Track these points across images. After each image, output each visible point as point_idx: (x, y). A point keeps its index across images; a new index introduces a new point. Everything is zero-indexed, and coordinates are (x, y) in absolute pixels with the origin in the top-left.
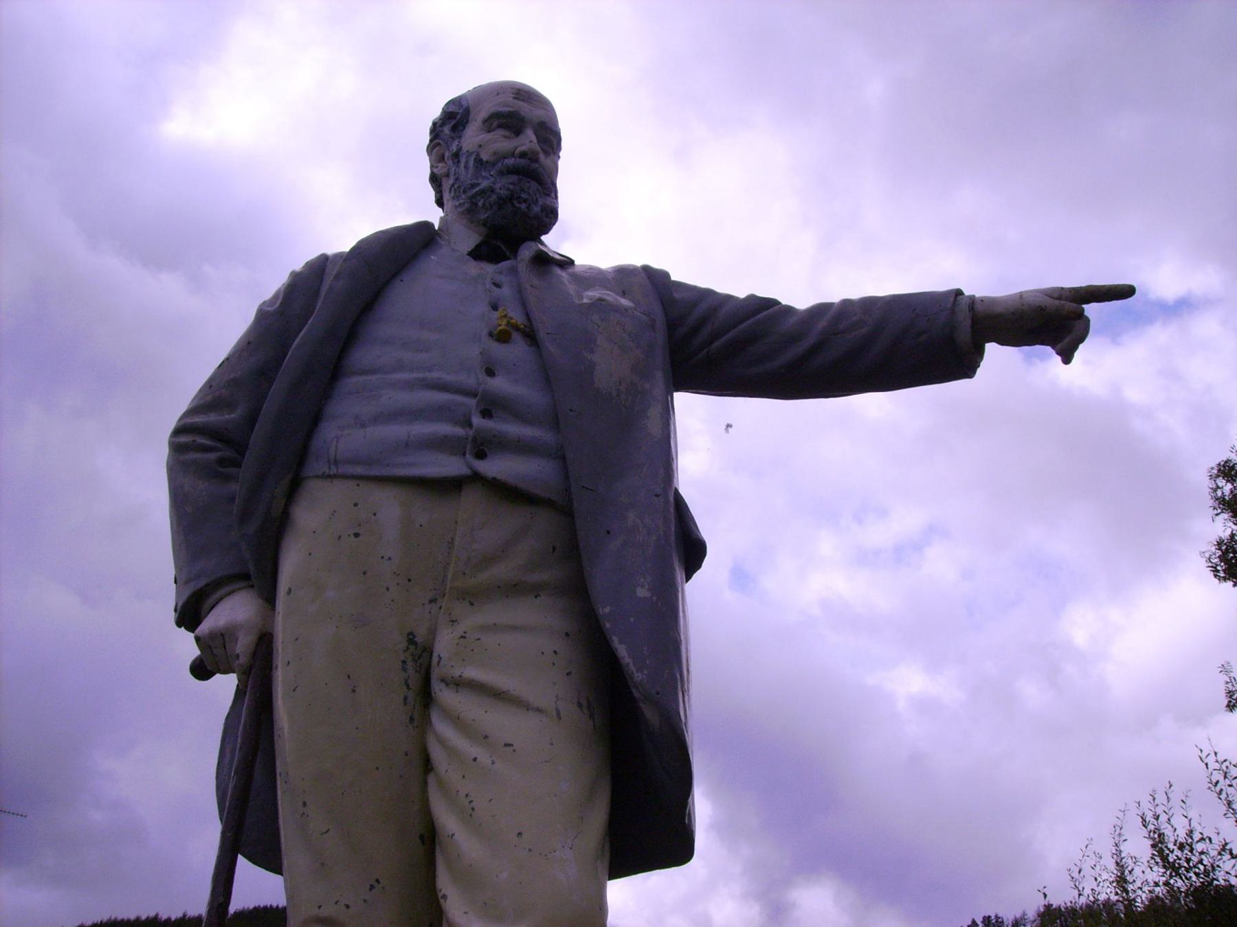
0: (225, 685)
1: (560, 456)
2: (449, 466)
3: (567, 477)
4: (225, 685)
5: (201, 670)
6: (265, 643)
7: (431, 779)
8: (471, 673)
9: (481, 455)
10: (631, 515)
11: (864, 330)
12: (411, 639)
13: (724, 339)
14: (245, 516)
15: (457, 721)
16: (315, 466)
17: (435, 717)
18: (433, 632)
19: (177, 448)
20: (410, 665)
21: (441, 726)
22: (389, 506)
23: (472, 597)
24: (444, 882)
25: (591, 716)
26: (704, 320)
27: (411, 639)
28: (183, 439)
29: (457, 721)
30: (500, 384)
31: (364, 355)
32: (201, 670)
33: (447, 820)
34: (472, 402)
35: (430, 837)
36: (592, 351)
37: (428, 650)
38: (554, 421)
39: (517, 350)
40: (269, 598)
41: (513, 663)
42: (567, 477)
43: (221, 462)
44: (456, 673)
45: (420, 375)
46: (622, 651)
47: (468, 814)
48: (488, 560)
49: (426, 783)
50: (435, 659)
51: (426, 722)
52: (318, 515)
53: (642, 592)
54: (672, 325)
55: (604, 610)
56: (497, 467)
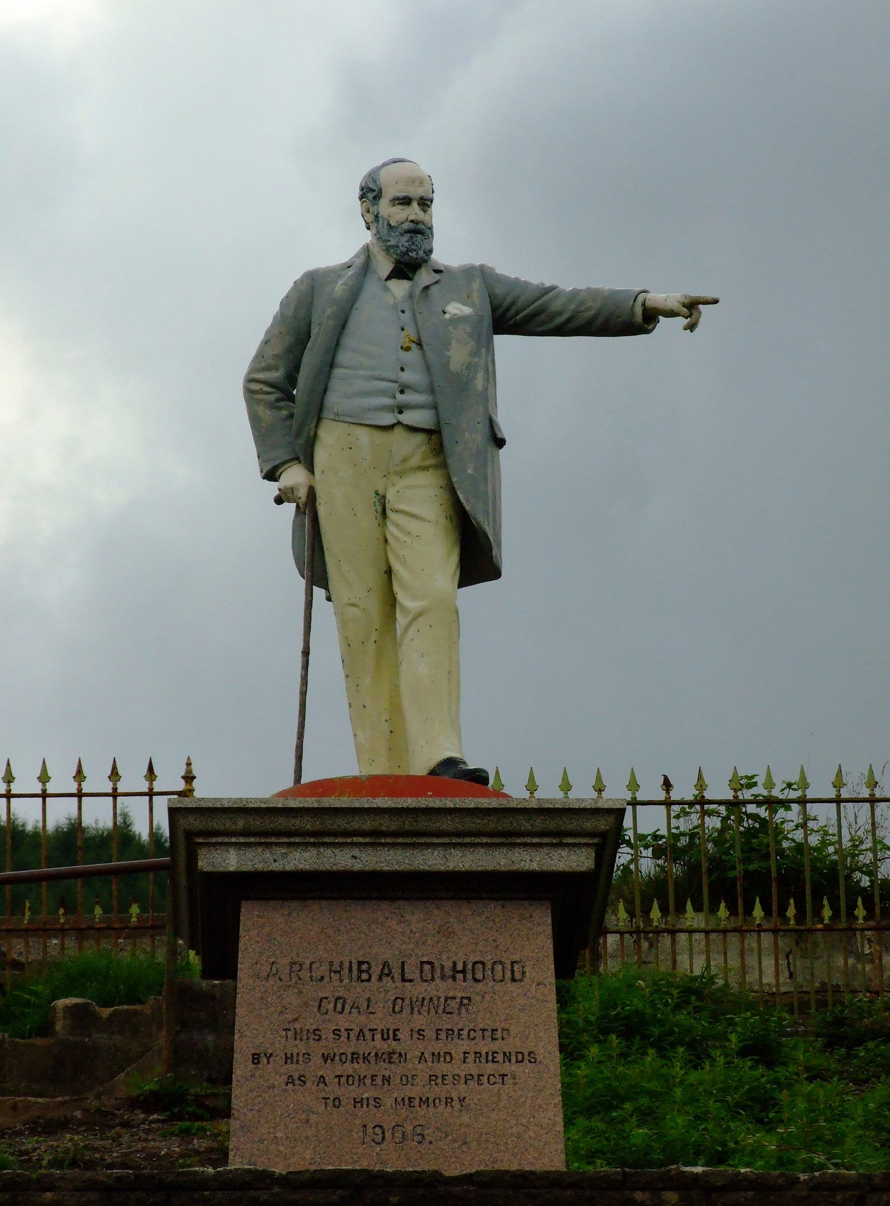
0: (289, 509)
1: (435, 407)
2: (388, 419)
3: (438, 416)
4: (289, 509)
5: (279, 501)
6: (312, 493)
7: (388, 548)
8: (402, 507)
9: (400, 412)
10: (467, 435)
11: (593, 312)
12: (377, 493)
13: (523, 314)
14: (298, 435)
15: (397, 526)
16: (325, 414)
17: (388, 523)
18: (386, 489)
19: (250, 394)
20: (377, 503)
21: (391, 528)
22: (364, 436)
23: (401, 474)
24: (396, 588)
25: (451, 522)
26: (513, 303)
27: (377, 493)
28: (255, 386)
29: (397, 526)
30: (406, 377)
31: (343, 357)
32: (279, 501)
33: (396, 566)
34: (395, 385)
35: (389, 572)
36: (449, 351)
37: (384, 497)
38: (432, 391)
39: (414, 355)
40: (311, 469)
41: (420, 502)
42: (438, 416)
43: (277, 400)
44: (396, 507)
45: (371, 373)
46: (461, 497)
47: (404, 562)
48: (405, 460)
49: (386, 550)
50: (387, 501)
51: (385, 524)
52: (330, 437)
53: (470, 471)
54: (494, 309)
55: (454, 479)
56: (408, 418)
